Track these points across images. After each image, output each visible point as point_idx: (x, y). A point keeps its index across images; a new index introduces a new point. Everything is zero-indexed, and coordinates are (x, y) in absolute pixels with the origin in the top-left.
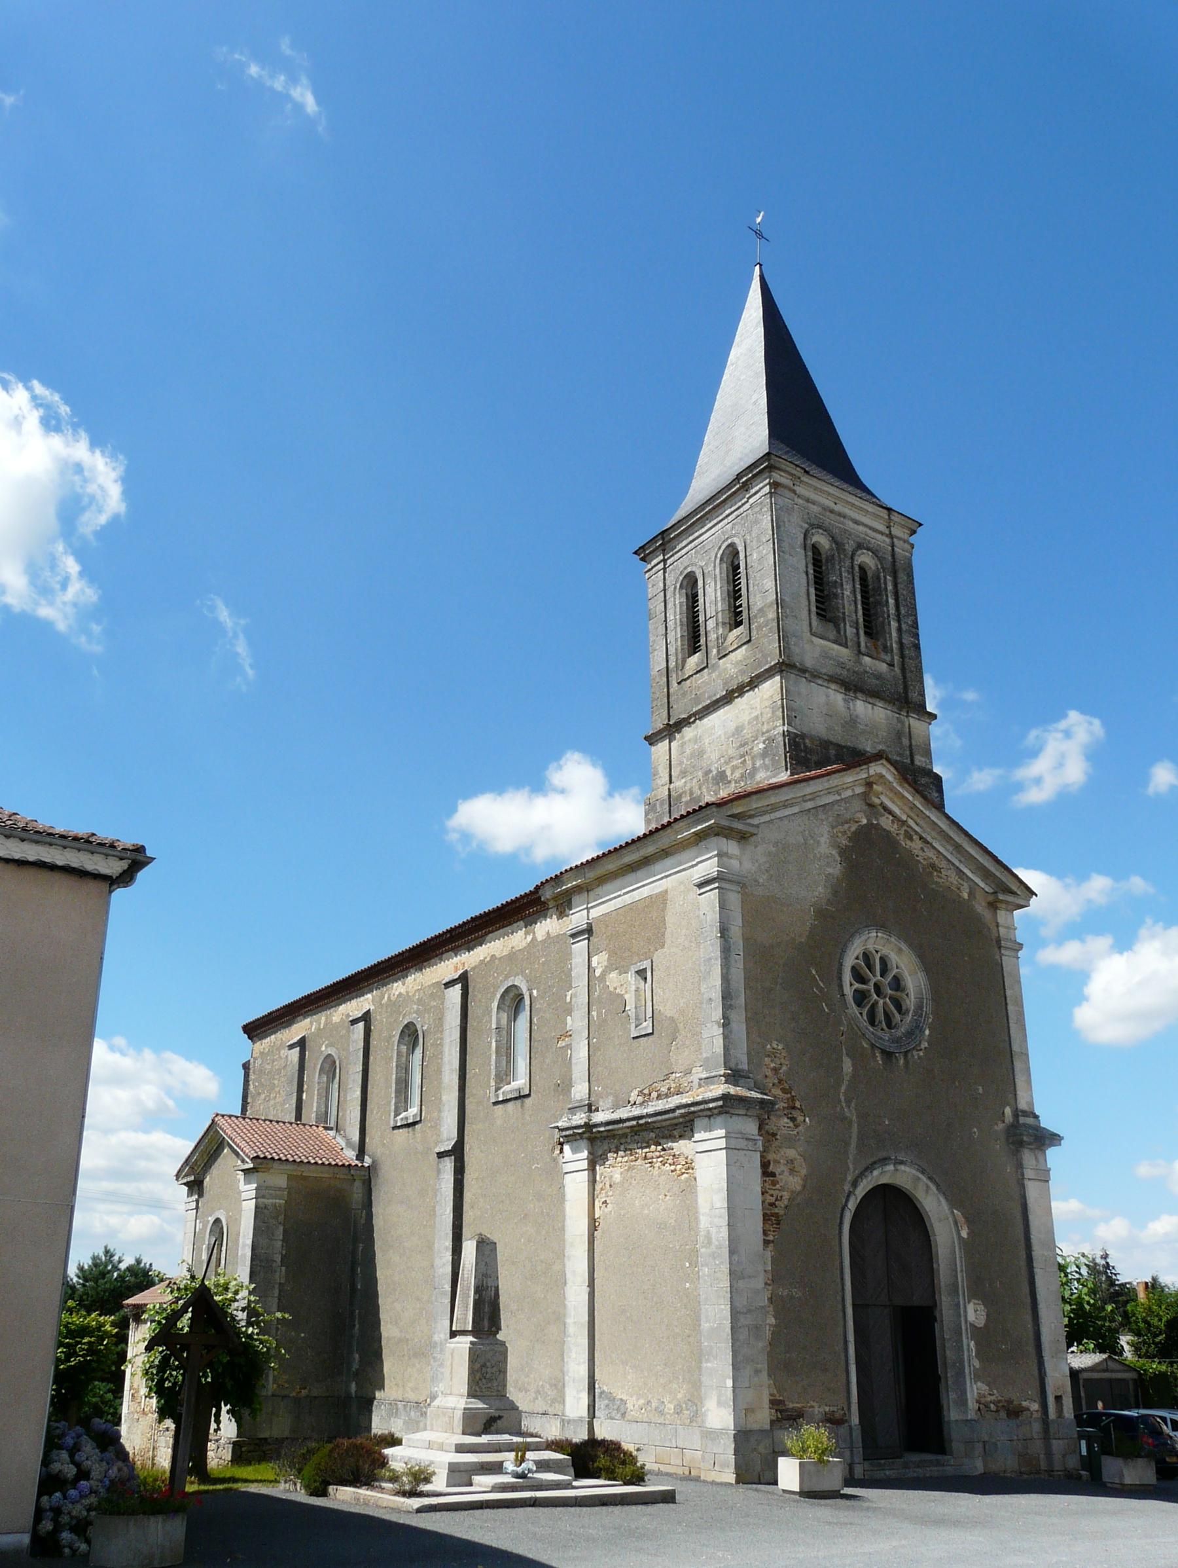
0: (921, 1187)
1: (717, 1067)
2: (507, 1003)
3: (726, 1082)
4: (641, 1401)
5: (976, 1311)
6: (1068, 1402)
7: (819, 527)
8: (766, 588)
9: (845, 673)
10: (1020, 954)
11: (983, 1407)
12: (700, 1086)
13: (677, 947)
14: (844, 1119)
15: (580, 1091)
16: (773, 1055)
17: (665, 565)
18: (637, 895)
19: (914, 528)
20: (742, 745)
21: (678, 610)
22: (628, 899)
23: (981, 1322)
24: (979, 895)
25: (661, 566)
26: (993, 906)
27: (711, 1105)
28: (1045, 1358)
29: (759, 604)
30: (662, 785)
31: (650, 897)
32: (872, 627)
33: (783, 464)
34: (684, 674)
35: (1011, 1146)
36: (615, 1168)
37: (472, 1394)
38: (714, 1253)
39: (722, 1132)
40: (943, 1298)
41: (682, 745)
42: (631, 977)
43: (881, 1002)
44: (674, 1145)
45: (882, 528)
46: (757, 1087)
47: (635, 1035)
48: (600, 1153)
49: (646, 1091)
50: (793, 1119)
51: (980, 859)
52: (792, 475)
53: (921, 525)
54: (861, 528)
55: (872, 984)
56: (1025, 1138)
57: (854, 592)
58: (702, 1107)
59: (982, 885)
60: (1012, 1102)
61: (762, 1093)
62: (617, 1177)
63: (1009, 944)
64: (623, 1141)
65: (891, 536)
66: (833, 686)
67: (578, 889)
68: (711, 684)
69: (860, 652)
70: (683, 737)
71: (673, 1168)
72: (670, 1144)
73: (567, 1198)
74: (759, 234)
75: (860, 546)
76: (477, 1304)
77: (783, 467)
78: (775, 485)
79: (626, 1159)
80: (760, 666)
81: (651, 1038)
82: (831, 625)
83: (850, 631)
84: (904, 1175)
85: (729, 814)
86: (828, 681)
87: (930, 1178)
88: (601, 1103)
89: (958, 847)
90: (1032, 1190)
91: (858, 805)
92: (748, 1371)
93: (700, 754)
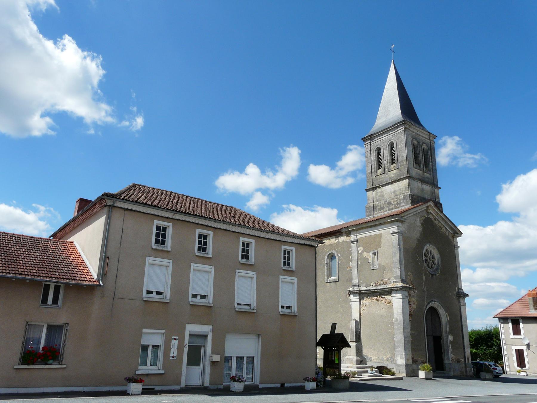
0: (439, 307)
1: (398, 279)
2: (330, 257)
3: (401, 283)
4: (376, 358)
5: (451, 337)
6: (470, 359)
7: (415, 139)
8: (403, 156)
9: (421, 177)
10: (459, 249)
11: (453, 360)
12: (394, 283)
13: (385, 248)
14: (424, 291)
15: (355, 281)
16: (409, 275)
17: (371, 144)
18: (372, 234)
19: (435, 137)
20: (396, 196)
21: (375, 156)
22: (369, 234)
23: (452, 340)
24: (450, 234)
25: (369, 144)
26: (453, 237)
27: (398, 288)
28: (465, 349)
29: (401, 159)
30: (371, 203)
31: (377, 235)
32: (426, 165)
33: (407, 123)
34: (377, 174)
35: (458, 297)
36: (367, 301)
37: (356, 356)
38: (398, 323)
39: (401, 295)
40: (444, 334)
41: (377, 193)
42: (371, 254)
43: (430, 262)
44: (385, 297)
45: (428, 138)
46: (407, 284)
47: (373, 269)
48: (362, 297)
49: (376, 283)
50: (414, 291)
51: (451, 225)
52: (409, 125)
53: (437, 136)
54: (423, 138)
55: (428, 257)
56: (461, 295)
57: (422, 156)
58: (395, 288)
59: (451, 231)
60: (458, 287)
61: (409, 285)
62: (367, 303)
63: (457, 247)
64: (369, 295)
65: (430, 140)
66: (419, 181)
67: (354, 230)
68: (386, 178)
69: (424, 172)
70: (377, 191)
71: (385, 302)
72: (384, 296)
73: (352, 308)
74: (393, 51)
75: (423, 143)
76: (356, 335)
77: (407, 123)
78: (405, 128)
79: (370, 299)
80: (401, 175)
81: (377, 270)
82: (417, 165)
83: (422, 166)
84: (435, 304)
85: (400, 216)
86: (418, 180)
87: (441, 305)
88: (362, 285)
89: (446, 222)
90: (462, 308)
91: (425, 212)
92: (407, 351)
93: (383, 196)
